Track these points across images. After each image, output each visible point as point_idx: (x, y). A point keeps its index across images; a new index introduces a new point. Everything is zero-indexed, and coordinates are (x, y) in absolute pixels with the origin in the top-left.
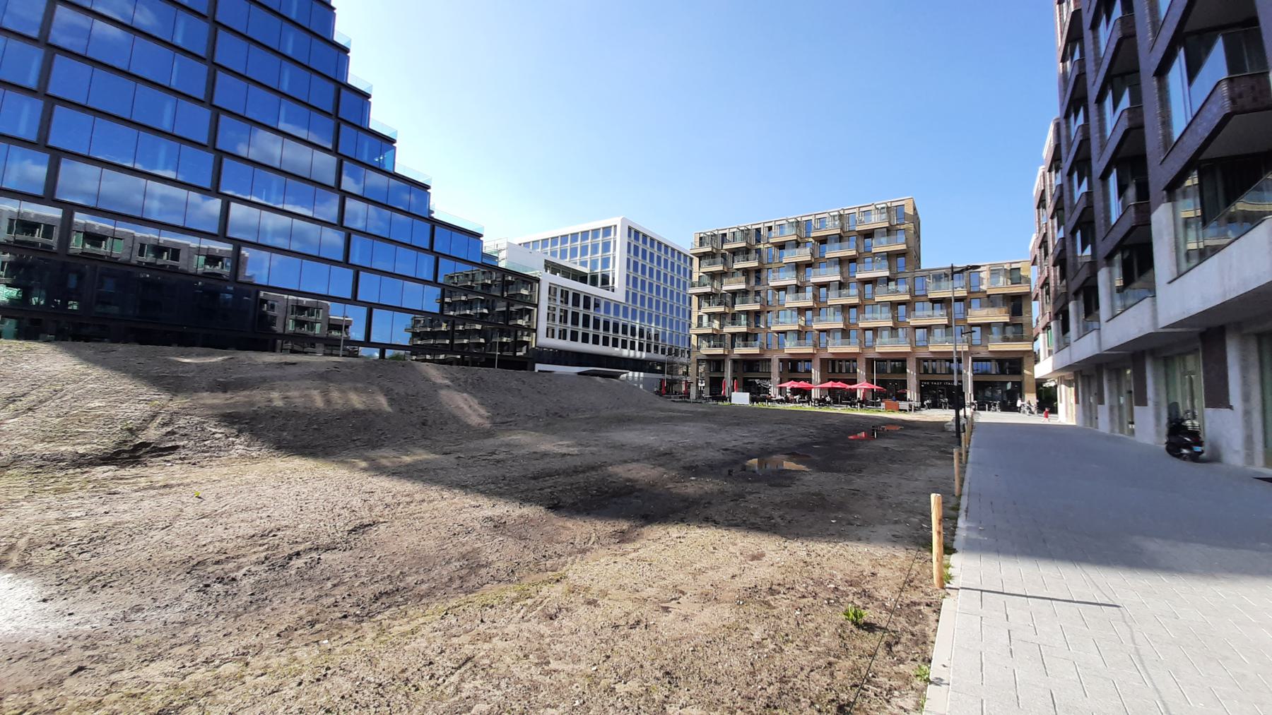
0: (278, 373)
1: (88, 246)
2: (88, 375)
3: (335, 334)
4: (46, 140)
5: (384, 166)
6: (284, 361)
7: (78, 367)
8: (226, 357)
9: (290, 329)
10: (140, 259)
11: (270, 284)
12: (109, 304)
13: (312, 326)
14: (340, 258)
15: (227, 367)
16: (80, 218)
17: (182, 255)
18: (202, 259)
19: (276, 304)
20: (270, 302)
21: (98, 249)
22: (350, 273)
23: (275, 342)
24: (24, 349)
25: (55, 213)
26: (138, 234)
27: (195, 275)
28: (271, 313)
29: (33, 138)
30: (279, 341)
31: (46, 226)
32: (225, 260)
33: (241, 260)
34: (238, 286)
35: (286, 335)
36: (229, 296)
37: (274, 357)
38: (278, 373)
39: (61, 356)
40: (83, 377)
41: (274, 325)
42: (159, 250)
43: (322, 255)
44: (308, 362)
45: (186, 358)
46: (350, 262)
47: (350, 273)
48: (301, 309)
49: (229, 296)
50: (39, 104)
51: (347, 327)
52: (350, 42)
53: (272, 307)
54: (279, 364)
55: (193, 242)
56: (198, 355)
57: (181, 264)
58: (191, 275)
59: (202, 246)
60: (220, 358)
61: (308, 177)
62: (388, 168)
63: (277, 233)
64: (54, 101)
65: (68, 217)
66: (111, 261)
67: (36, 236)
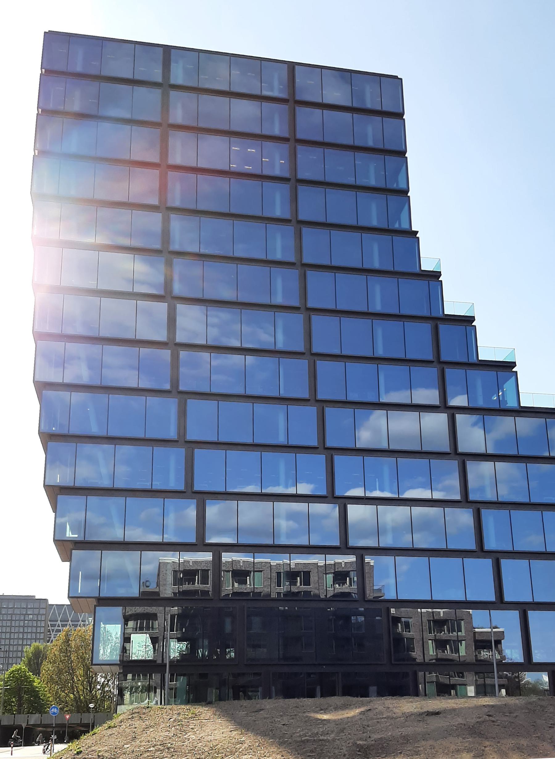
0: (420, 728)
1: (236, 585)
2: (242, 743)
3: (485, 654)
4: (192, 485)
5: (506, 402)
6: (425, 710)
7: (234, 733)
8: (362, 709)
9: (431, 653)
10: (278, 589)
11: (401, 597)
12: (259, 646)
13: (455, 645)
14: (472, 545)
15: (365, 723)
16: (227, 557)
17: (313, 578)
18: (330, 577)
19: (410, 620)
20: (403, 620)
21: (243, 586)
22: (487, 563)
23: (415, 674)
24: (190, 715)
25: (207, 556)
26: (274, 563)
27: (326, 600)
28: (406, 634)
29: (182, 488)
30: (421, 674)
31: (203, 571)
32: (352, 574)
33: (367, 569)
34: (367, 606)
35: (428, 664)
36: (361, 619)
37: (414, 705)
38: (420, 728)
39: (219, 721)
40: (238, 746)
41: (413, 650)
42: (292, 575)
43: (451, 546)
44: (454, 710)
45: (325, 713)
46: (486, 548)
47: (487, 563)
48: (439, 624)
49: (361, 619)
50: (182, 451)
51: (498, 642)
52: (439, 264)
53: (407, 626)
54: (421, 714)
55: (318, 560)
56: (337, 708)
57: (312, 588)
58: (322, 600)
59: (328, 562)
60: (358, 711)
61: (418, 448)
62: (511, 403)
63: (397, 530)
64: (193, 445)
65: (217, 558)
66: (256, 596)
67: (196, 584)
